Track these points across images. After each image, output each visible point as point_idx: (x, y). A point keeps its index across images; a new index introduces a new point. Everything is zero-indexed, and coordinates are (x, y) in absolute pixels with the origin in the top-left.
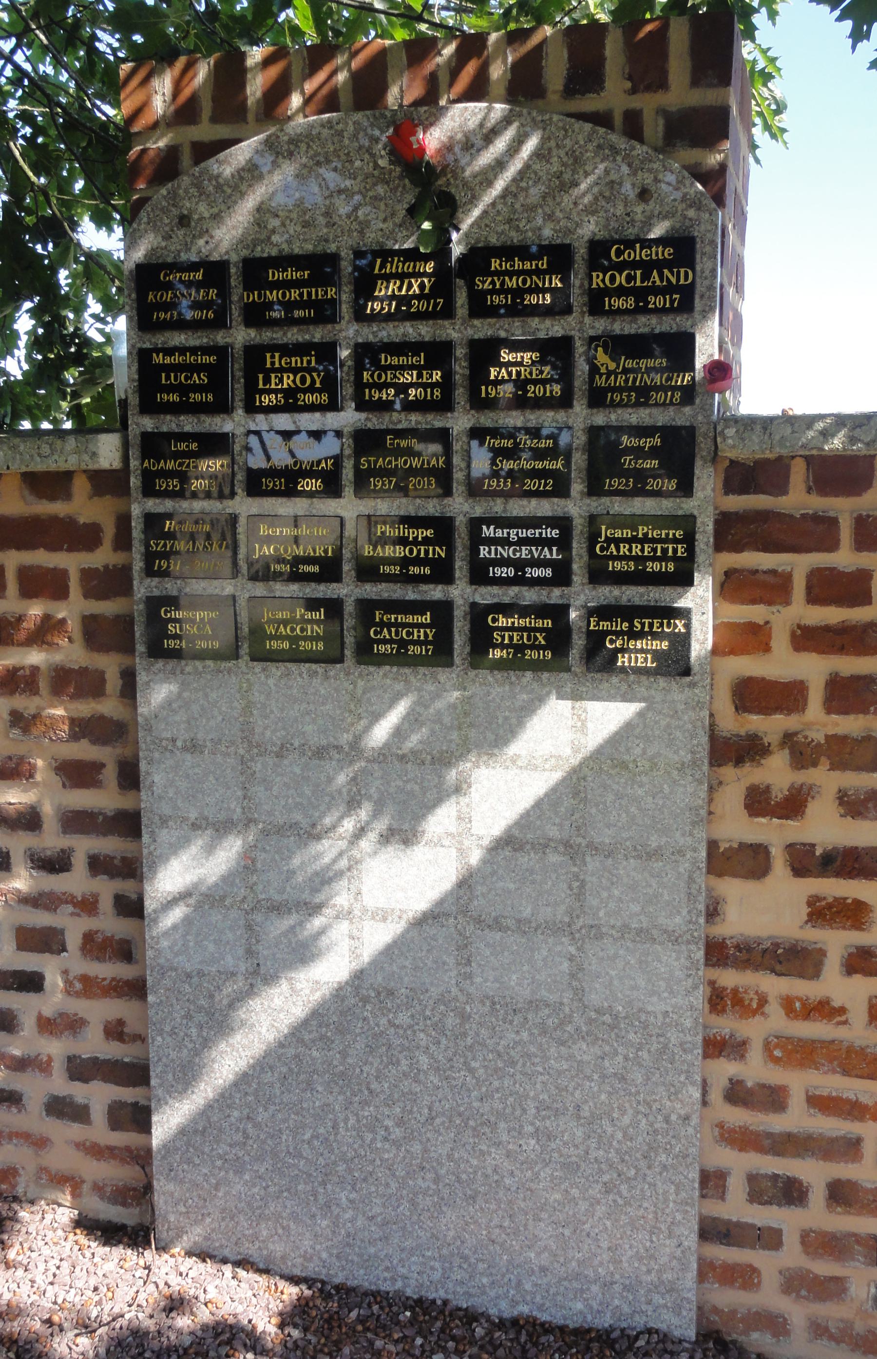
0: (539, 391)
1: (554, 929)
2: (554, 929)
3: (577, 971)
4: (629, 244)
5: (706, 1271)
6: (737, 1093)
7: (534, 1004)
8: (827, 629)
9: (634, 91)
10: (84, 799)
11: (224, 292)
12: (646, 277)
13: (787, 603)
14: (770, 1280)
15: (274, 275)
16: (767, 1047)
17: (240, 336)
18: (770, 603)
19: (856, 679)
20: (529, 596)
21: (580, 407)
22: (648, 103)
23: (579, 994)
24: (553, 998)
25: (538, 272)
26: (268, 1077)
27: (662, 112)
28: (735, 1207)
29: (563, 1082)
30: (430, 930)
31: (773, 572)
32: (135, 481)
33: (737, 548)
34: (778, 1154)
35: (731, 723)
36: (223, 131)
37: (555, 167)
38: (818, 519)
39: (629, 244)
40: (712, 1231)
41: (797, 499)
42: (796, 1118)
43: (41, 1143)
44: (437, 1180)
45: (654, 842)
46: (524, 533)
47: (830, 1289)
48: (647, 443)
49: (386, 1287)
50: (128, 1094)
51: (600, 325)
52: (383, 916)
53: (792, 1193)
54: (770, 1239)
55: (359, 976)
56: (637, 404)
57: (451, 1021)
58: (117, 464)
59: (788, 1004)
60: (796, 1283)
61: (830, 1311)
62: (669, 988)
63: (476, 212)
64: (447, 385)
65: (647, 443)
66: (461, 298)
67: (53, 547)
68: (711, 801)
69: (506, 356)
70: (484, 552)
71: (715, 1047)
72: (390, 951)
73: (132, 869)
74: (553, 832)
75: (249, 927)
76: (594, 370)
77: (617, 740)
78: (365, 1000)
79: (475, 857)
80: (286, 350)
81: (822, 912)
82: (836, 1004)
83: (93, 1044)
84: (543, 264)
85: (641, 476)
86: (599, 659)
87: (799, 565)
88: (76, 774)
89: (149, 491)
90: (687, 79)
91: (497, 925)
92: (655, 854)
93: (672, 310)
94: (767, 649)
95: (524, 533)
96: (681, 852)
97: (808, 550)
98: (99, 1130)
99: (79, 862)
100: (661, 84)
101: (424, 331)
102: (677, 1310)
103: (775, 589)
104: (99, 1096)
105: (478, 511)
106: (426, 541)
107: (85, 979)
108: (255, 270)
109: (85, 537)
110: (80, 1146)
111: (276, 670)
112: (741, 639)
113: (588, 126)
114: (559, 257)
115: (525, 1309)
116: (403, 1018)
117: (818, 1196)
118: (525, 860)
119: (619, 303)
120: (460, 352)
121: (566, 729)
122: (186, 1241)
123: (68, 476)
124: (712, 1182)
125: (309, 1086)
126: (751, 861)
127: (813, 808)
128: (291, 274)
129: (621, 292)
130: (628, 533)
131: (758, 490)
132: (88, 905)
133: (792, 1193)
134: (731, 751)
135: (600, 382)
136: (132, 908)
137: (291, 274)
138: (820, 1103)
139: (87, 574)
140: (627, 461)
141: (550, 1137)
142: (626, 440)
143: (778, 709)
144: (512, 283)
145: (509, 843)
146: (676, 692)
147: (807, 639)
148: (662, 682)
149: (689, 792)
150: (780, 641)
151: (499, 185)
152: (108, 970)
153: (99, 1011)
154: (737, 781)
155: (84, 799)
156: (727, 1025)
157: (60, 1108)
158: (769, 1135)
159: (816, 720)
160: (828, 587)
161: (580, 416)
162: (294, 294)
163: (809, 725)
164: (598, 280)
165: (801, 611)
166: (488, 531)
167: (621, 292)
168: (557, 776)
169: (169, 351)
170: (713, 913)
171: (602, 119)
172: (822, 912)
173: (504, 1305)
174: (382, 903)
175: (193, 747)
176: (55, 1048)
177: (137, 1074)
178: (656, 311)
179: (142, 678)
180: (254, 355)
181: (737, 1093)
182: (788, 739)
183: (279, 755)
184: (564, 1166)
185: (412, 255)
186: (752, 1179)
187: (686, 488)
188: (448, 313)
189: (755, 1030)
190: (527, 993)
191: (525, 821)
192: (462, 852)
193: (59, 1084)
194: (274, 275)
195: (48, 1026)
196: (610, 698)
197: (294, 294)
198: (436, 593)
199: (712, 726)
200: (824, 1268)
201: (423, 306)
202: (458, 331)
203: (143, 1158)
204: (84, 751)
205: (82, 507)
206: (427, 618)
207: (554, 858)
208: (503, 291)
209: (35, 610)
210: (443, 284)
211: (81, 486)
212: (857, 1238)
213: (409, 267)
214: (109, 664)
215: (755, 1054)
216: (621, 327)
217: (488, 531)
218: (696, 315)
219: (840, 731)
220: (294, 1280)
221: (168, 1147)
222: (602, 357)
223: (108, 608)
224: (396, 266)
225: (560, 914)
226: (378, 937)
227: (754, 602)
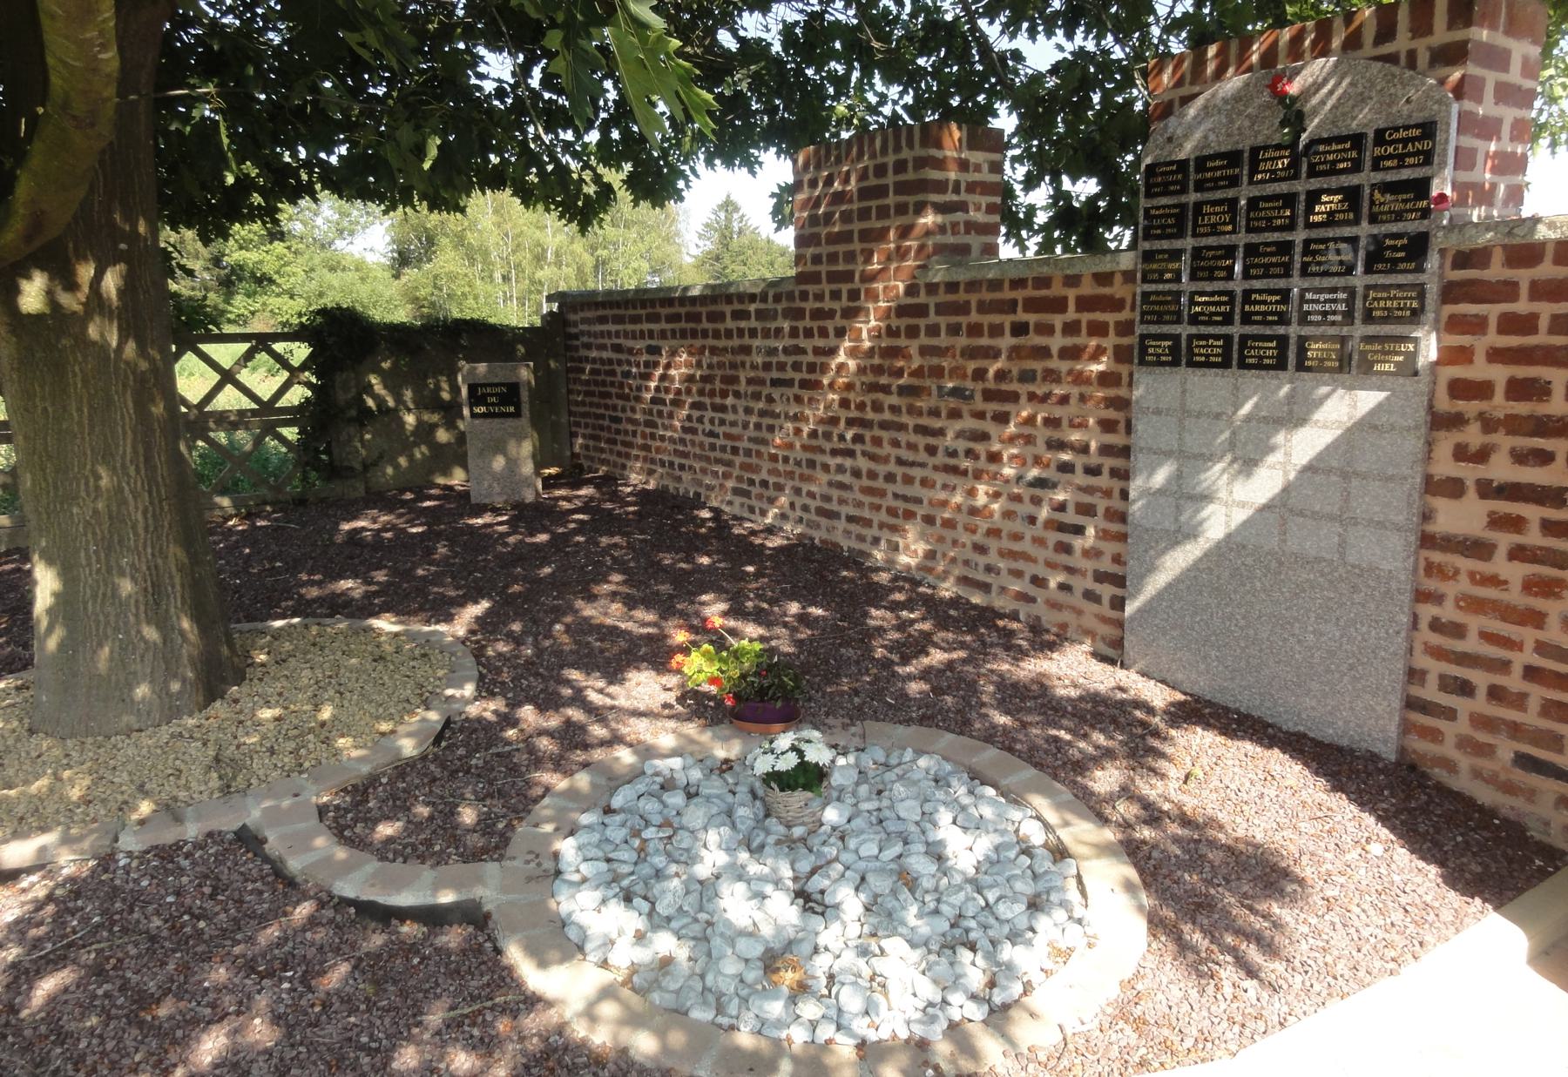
0: (1341, 216)
1: (1331, 518)
2: (1331, 518)
3: (1343, 544)
4: (1397, 129)
5: (1406, 728)
6: (1436, 625)
7: (1318, 560)
8: (1509, 349)
9: (1413, 38)
10: (1111, 439)
11: (1186, 176)
12: (1405, 147)
13: (1485, 334)
14: (1450, 740)
15: (1210, 164)
16: (1457, 600)
17: (1193, 197)
18: (1473, 334)
19: (1526, 380)
20: (1332, 331)
21: (1365, 224)
22: (1422, 46)
23: (1342, 555)
24: (1328, 557)
25: (1344, 150)
26: (1181, 586)
27: (1430, 48)
28: (1429, 691)
29: (1330, 604)
30: (1266, 514)
31: (1476, 316)
32: (1139, 275)
33: (1456, 301)
34: (1458, 664)
35: (1444, 404)
36: (1197, 89)
37: (1360, 89)
38: (1506, 283)
39: (1397, 129)
40: (1412, 704)
41: (1496, 271)
42: (1472, 644)
43: (1079, 612)
44: (1261, 651)
45: (1390, 471)
46: (1328, 296)
47: (1485, 750)
48: (1399, 243)
49: (1231, 705)
50: (1119, 592)
51: (1378, 177)
52: (1243, 505)
53: (1466, 689)
54: (1451, 714)
55: (1229, 536)
56: (1396, 220)
57: (1274, 565)
58: (1131, 267)
59: (1472, 575)
60: (1464, 743)
61: (1485, 764)
62: (1392, 555)
63: (1316, 121)
64: (1293, 218)
65: (1399, 243)
66: (1304, 168)
67: (1103, 310)
68: (1430, 452)
69: (1325, 198)
70: (1306, 307)
71: (1422, 596)
72: (1246, 524)
73: (1124, 475)
74: (1335, 464)
75: (1177, 507)
76: (1372, 203)
77: (1373, 413)
78: (1231, 550)
79: (1292, 476)
80: (1214, 203)
81: (1497, 522)
82: (1502, 578)
83: (1106, 565)
84: (1348, 145)
85: (1395, 261)
86: (1367, 367)
87: (1493, 311)
88: (1107, 426)
89: (1145, 280)
90: (1445, 26)
91: (1301, 514)
92: (1391, 478)
93: (1419, 165)
94: (1471, 361)
95: (1328, 296)
96: (1405, 478)
97: (1499, 302)
98: (1106, 609)
99: (1106, 471)
100: (1429, 31)
101: (1284, 187)
102: (1385, 742)
103: (1477, 325)
104: (1107, 591)
105: (1306, 285)
106: (1277, 302)
107: (1104, 531)
108: (1201, 162)
109: (1117, 305)
110: (1096, 616)
111: (1199, 372)
112: (1451, 356)
113: (1379, 64)
114: (1357, 140)
115: (1302, 729)
116: (1249, 561)
117: (1482, 692)
118: (1318, 478)
119: (1389, 163)
120: (1302, 197)
121: (1343, 407)
122: (1138, 666)
123: (1112, 274)
124: (1415, 675)
125: (1201, 593)
126: (1454, 488)
127: (1494, 458)
128: (1218, 163)
129: (1390, 157)
130: (1385, 295)
131: (1473, 267)
132: (1108, 494)
133: (1466, 689)
134: (1440, 422)
135: (1376, 209)
136: (1124, 495)
137: (1218, 163)
138: (1487, 637)
139: (1117, 324)
140: (1388, 254)
141: (1322, 634)
142: (1388, 242)
143: (1474, 398)
144: (1331, 157)
145: (1310, 469)
146: (1408, 384)
147: (1496, 355)
148: (1401, 380)
149: (1413, 444)
150: (1480, 357)
151: (1328, 106)
152: (1115, 527)
153: (1110, 548)
154: (1446, 443)
155: (1111, 439)
156: (1432, 585)
157: (1090, 596)
158: (1454, 653)
159: (1500, 405)
160: (1510, 324)
161: (1365, 229)
162: (1218, 173)
163: (1495, 408)
164: (1378, 151)
165: (1493, 339)
166: (1309, 296)
167: (1390, 157)
168: (1339, 432)
169: (1158, 208)
170: (1427, 516)
171: (1392, 59)
172: (1497, 522)
173: (1290, 724)
174: (1242, 499)
175: (1158, 412)
176: (1089, 565)
177: (1120, 581)
178: (1410, 166)
179: (1136, 376)
180: (1198, 206)
181: (1436, 625)
182: (1481, 416)
183: (1198, 417)
184: (1328, 652)
185: (1278, 147)
186: (1442, 677)
187: (1420, 269)
188: (1296, 177)
189: (1450, 589)
190: (1313, 553)
191: (1320, 457)
192: (1286, 473)
193: (1089, 583)
194: (1210, 164)
195: (1086, 553)
196: (1371, 389)
197: (1218, 173)
198: (1281, 330)
199: (1431, 407)
200: (1483, 737)
201: (1282, 174)
202: (1301, 187)
203: (1120, 624)
204: (1111, 414)
205: (1118, 289)
206: (1274, 344)
207: (1334, 478)
208: (1325, 162)
209: (1093, 342)
210: (1294, 164)
211: (1118, 279)
212: (1504, 721)
213: (1277, 154)
214: (1124, 370)
215: (1449, 604)
216: (1391, 177)
217: (1309, 296)
218: (1435, 166)
219: (1514, 412)
220: (1185, 694)
221: (1132, 618)
222: (1377, 195)
223: (1125, 341)
224: (1270, 154)
225: (1336, 511)
226: (1240, 516)
227: (1464, 333)
